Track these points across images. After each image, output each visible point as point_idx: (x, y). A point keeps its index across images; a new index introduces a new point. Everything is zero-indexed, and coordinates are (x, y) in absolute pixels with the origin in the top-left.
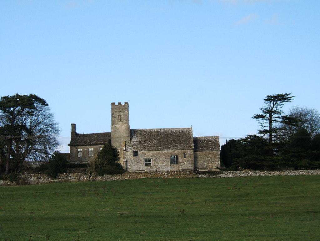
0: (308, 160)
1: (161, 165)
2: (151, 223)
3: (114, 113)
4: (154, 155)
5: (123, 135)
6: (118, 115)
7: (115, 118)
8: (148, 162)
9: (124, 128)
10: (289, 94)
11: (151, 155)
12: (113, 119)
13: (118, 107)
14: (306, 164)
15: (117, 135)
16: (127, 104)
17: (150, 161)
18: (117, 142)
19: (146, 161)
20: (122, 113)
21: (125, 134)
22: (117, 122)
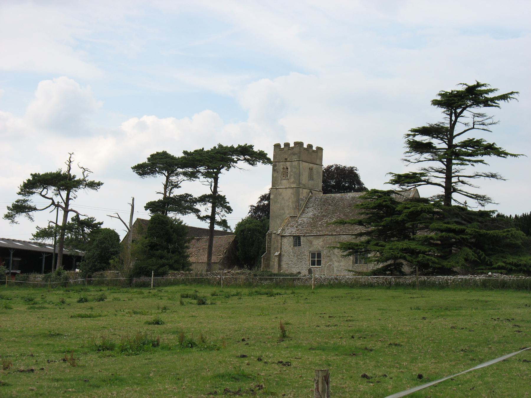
0: (475, 223)
1: (336, 264)
2: (229, 320)
3: (277, 163)
4: (325, 244)
5: (288, 206)
6: (282, 167)
7: (278, 172)
8: (316, 259)
9: (290, 191)
10: (483, 85)
11: (321, 243)
12: (275, 175)
13: (283, 151)
14: (276, 168)
15: (279, 205)
16: (320, 149)
17: (319, 255)
18: (278, 219)
19: (313, 255)
20: (288, 164)
21: (290, 204)
22: (279, 181)
